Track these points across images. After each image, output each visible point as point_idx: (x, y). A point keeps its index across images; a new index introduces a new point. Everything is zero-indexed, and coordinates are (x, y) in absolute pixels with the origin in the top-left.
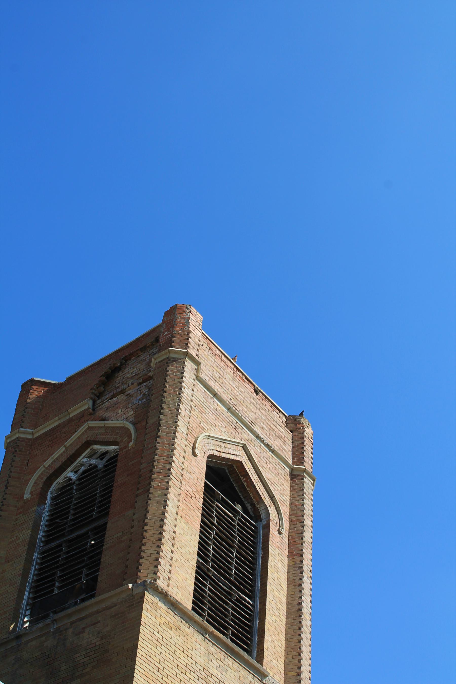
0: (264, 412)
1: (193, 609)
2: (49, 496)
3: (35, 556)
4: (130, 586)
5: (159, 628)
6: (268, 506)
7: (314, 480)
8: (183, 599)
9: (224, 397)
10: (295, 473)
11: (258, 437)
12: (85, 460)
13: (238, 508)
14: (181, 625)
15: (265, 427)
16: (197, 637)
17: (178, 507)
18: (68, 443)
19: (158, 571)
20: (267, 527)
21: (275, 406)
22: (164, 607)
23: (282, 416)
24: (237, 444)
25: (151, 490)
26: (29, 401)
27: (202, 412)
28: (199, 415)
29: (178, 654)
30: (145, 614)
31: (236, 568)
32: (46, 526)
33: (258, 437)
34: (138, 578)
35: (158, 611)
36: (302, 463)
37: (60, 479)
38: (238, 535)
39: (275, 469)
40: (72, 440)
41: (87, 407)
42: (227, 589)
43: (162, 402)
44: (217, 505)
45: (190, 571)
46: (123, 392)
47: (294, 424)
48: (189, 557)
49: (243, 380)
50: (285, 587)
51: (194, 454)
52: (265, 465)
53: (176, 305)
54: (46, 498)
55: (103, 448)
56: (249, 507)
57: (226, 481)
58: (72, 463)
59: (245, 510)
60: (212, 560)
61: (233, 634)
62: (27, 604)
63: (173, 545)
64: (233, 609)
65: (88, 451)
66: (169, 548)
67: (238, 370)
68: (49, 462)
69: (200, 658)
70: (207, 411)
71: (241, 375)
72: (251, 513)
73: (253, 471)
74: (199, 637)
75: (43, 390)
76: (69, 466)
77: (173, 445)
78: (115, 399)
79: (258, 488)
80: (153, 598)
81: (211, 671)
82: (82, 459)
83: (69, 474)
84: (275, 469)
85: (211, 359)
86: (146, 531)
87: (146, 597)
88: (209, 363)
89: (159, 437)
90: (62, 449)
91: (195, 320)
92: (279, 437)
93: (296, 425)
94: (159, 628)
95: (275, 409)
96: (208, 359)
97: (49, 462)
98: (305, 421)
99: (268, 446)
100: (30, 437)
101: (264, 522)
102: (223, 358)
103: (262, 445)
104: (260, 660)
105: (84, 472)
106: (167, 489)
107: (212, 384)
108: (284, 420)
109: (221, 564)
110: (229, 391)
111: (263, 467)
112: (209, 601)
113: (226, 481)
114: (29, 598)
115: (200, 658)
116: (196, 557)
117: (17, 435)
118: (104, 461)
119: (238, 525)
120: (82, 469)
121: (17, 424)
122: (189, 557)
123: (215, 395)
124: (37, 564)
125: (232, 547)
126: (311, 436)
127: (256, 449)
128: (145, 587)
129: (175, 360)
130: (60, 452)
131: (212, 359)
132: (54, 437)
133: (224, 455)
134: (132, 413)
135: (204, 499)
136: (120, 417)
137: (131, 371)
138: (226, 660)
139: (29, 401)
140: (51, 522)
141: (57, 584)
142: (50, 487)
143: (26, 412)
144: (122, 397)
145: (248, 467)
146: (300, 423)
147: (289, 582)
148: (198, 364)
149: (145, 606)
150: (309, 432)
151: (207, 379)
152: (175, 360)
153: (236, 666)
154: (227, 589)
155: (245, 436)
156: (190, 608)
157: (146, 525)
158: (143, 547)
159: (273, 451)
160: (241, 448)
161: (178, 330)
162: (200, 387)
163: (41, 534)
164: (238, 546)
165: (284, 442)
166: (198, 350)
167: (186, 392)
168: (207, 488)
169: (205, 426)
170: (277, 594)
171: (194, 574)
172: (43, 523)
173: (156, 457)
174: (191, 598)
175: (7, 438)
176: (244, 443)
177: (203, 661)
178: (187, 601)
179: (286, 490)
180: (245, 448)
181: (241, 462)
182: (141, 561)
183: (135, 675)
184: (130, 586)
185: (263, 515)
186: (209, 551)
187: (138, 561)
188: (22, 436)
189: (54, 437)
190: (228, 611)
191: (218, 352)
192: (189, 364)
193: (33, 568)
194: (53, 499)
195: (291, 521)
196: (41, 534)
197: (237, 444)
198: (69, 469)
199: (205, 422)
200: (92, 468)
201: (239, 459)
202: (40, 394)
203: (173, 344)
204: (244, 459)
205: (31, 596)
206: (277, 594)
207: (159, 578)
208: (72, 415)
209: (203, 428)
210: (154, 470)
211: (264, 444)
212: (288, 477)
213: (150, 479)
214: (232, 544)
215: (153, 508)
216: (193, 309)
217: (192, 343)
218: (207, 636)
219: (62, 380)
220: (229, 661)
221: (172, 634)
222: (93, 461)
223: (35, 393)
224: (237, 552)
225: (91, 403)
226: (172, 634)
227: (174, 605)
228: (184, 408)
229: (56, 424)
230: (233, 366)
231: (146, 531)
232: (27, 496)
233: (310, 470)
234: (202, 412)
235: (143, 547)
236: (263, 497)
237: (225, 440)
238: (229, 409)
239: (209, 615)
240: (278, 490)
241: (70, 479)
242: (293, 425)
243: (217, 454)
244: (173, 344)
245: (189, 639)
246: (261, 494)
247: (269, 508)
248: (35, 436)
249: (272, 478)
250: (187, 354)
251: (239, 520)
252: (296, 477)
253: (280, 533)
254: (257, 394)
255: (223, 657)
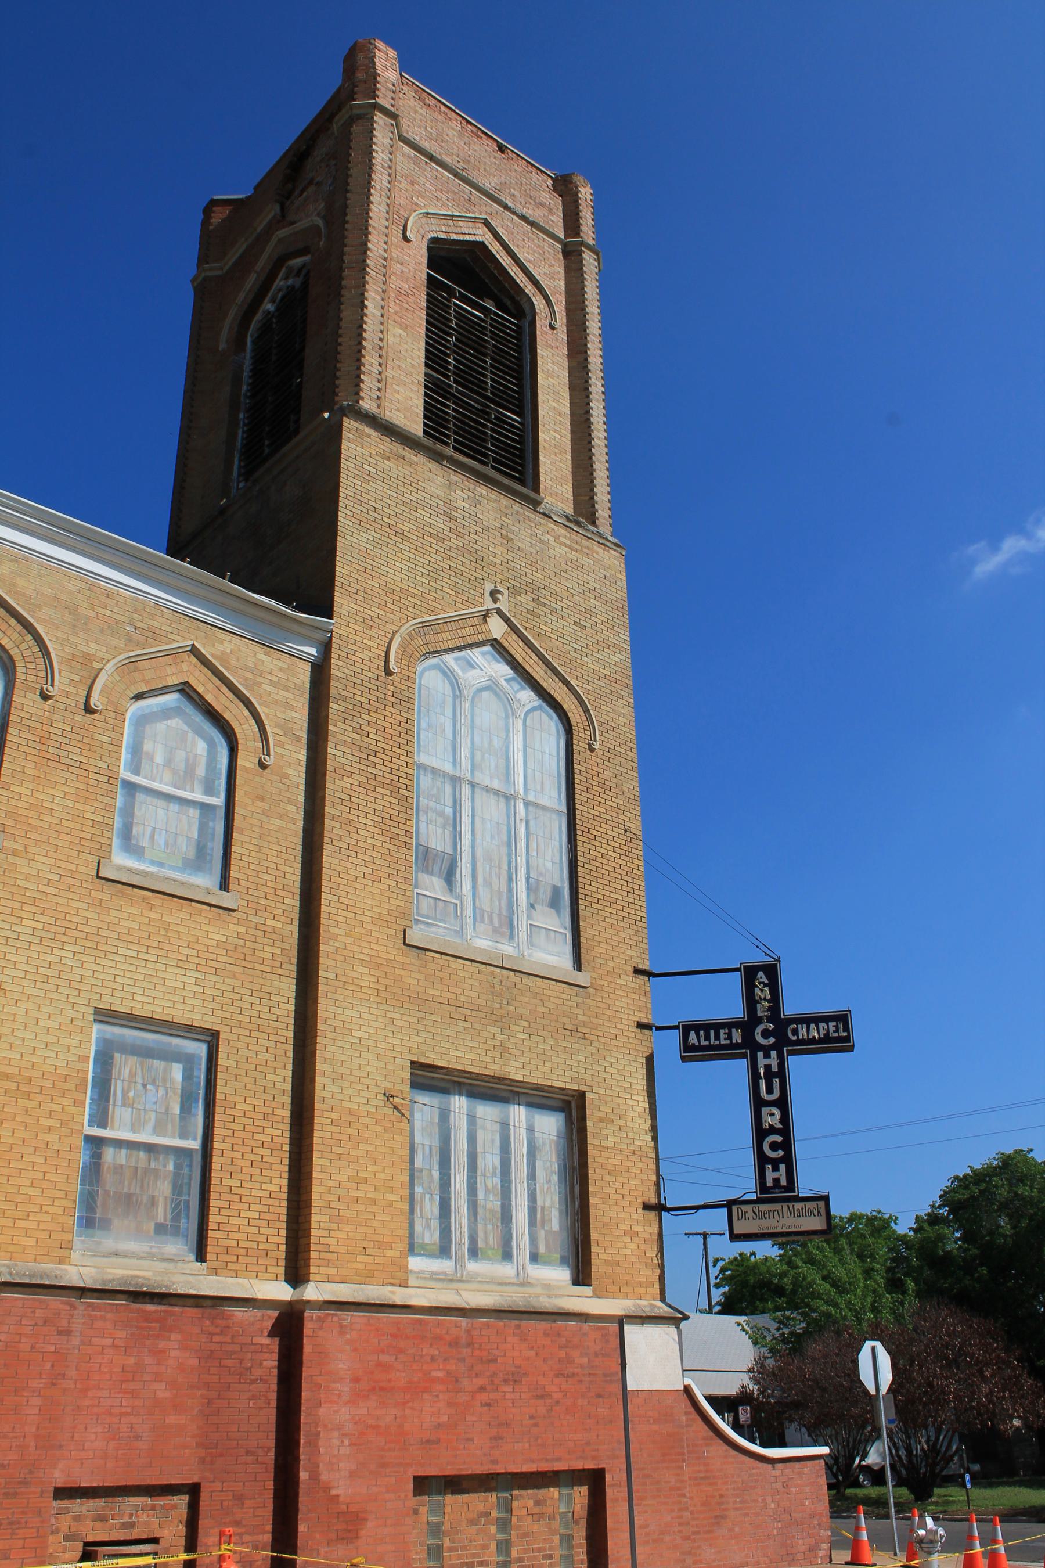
0: (513, 174)
1: (425, 432)
2: (249, 340)
3: (241, 416)
4: (326, 415)
5: (370, 459)
6: (531, 295)
7: (597, 254)
8: (408, 423)
9: (448, 160)
10: (569, 248)
11: (506, 207)
12: (282, 283)
13: (489, 305)
14: (403, 453)
15: (516, 193)
16: (430, 466)
17: (382, 307)
18: (259, 266)
19: (361, 390)
20: (533, 323)
21: (533, 165)
22: (374, 433)
23: (545, 177)
24: (474, 220)
25: (343, 292)
26: (211, 228)
27: (412, 183)
28: (410, 188)
29: (402, 489)
30: (345, 444)
31: (492, 380)
32: (250, 377)
33: (506, 207)
34: (336, 403)
35: (366, 439)
36: (578, 235)
37: (259, 316)
38: (491, 338)
39: (539, 246)
40: (263, 262)
41: (272, 214)
42: (480, 407)
43: (348, 176)
44: (456, 305)
45: (415, 389)
46: (311, 182)
47: (564, 187)
48: (412, 370)
49: (478, 136)
50: (567, 395)
51: (406, 239)
52: (521, 243)
53: (356, 44)
54: (246, 343)
55: (298, 262)
56: (508, 303)
57: (462, 271)
58: (268, 290)
59: (500, 306)
60: (454, 373)
61: (495, 460)
62: (239, 475)
63: (380, 356)
64: (492, 430)
65: (284, 270)
66: (375, 361)
67: (468, 122)
68: (242, 296)
69: (436, 491)
70: (422, 180)
71: (474, 130)
72: (513, 311)
73: (503, 253)
74: (433, 465)
75: (227, 210)
76: (265, 296)
77: (367, 229)
78: (305, 194)
79: (513, 274)
80: (356, 424)
81: (456, 505)
82: (279, 283)
83: (269, 306)
84: (539, 246)
85: (420, 111)
86: (340, 344)
87: (344, 424)
88: (418, 117)
89: (347, 222)
90: (253, 277)
91: (386, 62)
92: (542, 205)
93: (566, 186)
94: (370, 459)
95: (534, 170)
96: (416, 112)
97: (242, 296)
98: (579, 179)
99: (523, 218)
100: (219, 273)
101: (529, 318)
102: (443, 108)
103: (515, 217)
104: (536, 489)
105: (283, 298)
106: (364, 286)
107: (426, 145)
108: (550, 182)
109: (469, 377)
110: (455, 151)
111: (518, 246)
112: (454, 425)
113: (462, 271)
114: (240, 467)
115: (436, 491)
116: (423, 369)
117: (203, 275)
118: (302, 277)
119: (491, 325)
120: (280, 295)
121: (203, 259)
122: (412, 370)
123: (431, 158)
124: (245, 425)
125: (485, 355)
126: (589, 197)
127: (504, 223)
128: (343, 412)
129: (359, 117)
130: (251, 281)
131: (423, 111)
132: (244, 265)
133: (454, 237)
134: (323, 205)
135: (428, 294)
136: (310, 216)
137: (320, 152)
138: (478, 489)
139: (211, 228)
140: (256, 372)
141: (267, 442)
142: (248, 328)
143: (212, 242)
144: (311, 189)
145: (495, 248)
146: (571, 182)
147: (572, 388)
148: (394, 116)
149: (345, 434)
150: (585, 193)
151: (417, 138)
152: (359, 117)
153: (494, 495)
154: (480, 407)
155: (486, 208)
156: (420, 433)
157: (340, 336)
158: (338, 365)
159: (532, 224)
160: (480, 225)
161: (361, 75)
162: (407, 149)
163: (244, 388)
164: (493, 352)
165: (550, 211)
166: (393, 99)
167: (380, 157)
168: (431, 281)
169: (420, 201)
170: (554, 404)
171: (422, 390)
172: (245, 374)
173: (346, 249)
174: (421, 419)
175: (193, 281)
176: (484, 216)
177: (442, 494)
178: (416, 427)
179: (559, 273)
180: (487, 224)
181: (483, 243)
182: (337, 382)
183: (340, 518)
184: (326, 415)
185: (527, 309)
186: (449, 363)
187: (334, 383)
188: (208, 274)
189: (244, 265)
190: (486, 434)
191: (433, 102)
192: (379, 118)
193: (240, 432)
194: (253, 342)
195: (568, 311)
196: (244, 388)
197: (474, 220)
198: (266, 300)
199: (420, 195)
200: (291, 289)
201: (479, 239)
202: (225, 216)
203: (355, 96)
204: (488, 239)
205: (242, 464)
206: (554, 404)
207: (363, 399)
208: (259, 229)
209: (416, 204)
210: (344, 266)
211: (518, 216)
212: (561, 256)
213: (341, 278)
214: (484, 350)
215: (347, 314)
216: (379, 44)
217: (383, 90)
218: (445, 462)
219: (250, 192)
220: (483, 490)
221: (392, 465)
222: (290, 282)
223: (219, 216)
224: (492, 359)
225: (277, 207)
226: (392, 465)
227: (388, 430)
228: (380, 179)
229: (245, 246)
230: (459, 118)
231: (340, 344)
232: (222, 346)
233: (591, 242)
234: (412, 183)
235: (338, 365)
236: (522, 285)
237: (453, 216)
238: (456, 175)
239: (455, 440)
240: (545, 274)
241: (269, 312)
242: (563, 187)
243: (443, 236)
244: (355, 96)
245: (418, 468)
246: (518, 281)
247: (533, 299)
248: (227, 268)
249: (536, 262)
250: (376, 106)
251: (492, 319)
252: (571, 254)
253: (552, 328)
254: (502, 152)
255: (472, 486)
